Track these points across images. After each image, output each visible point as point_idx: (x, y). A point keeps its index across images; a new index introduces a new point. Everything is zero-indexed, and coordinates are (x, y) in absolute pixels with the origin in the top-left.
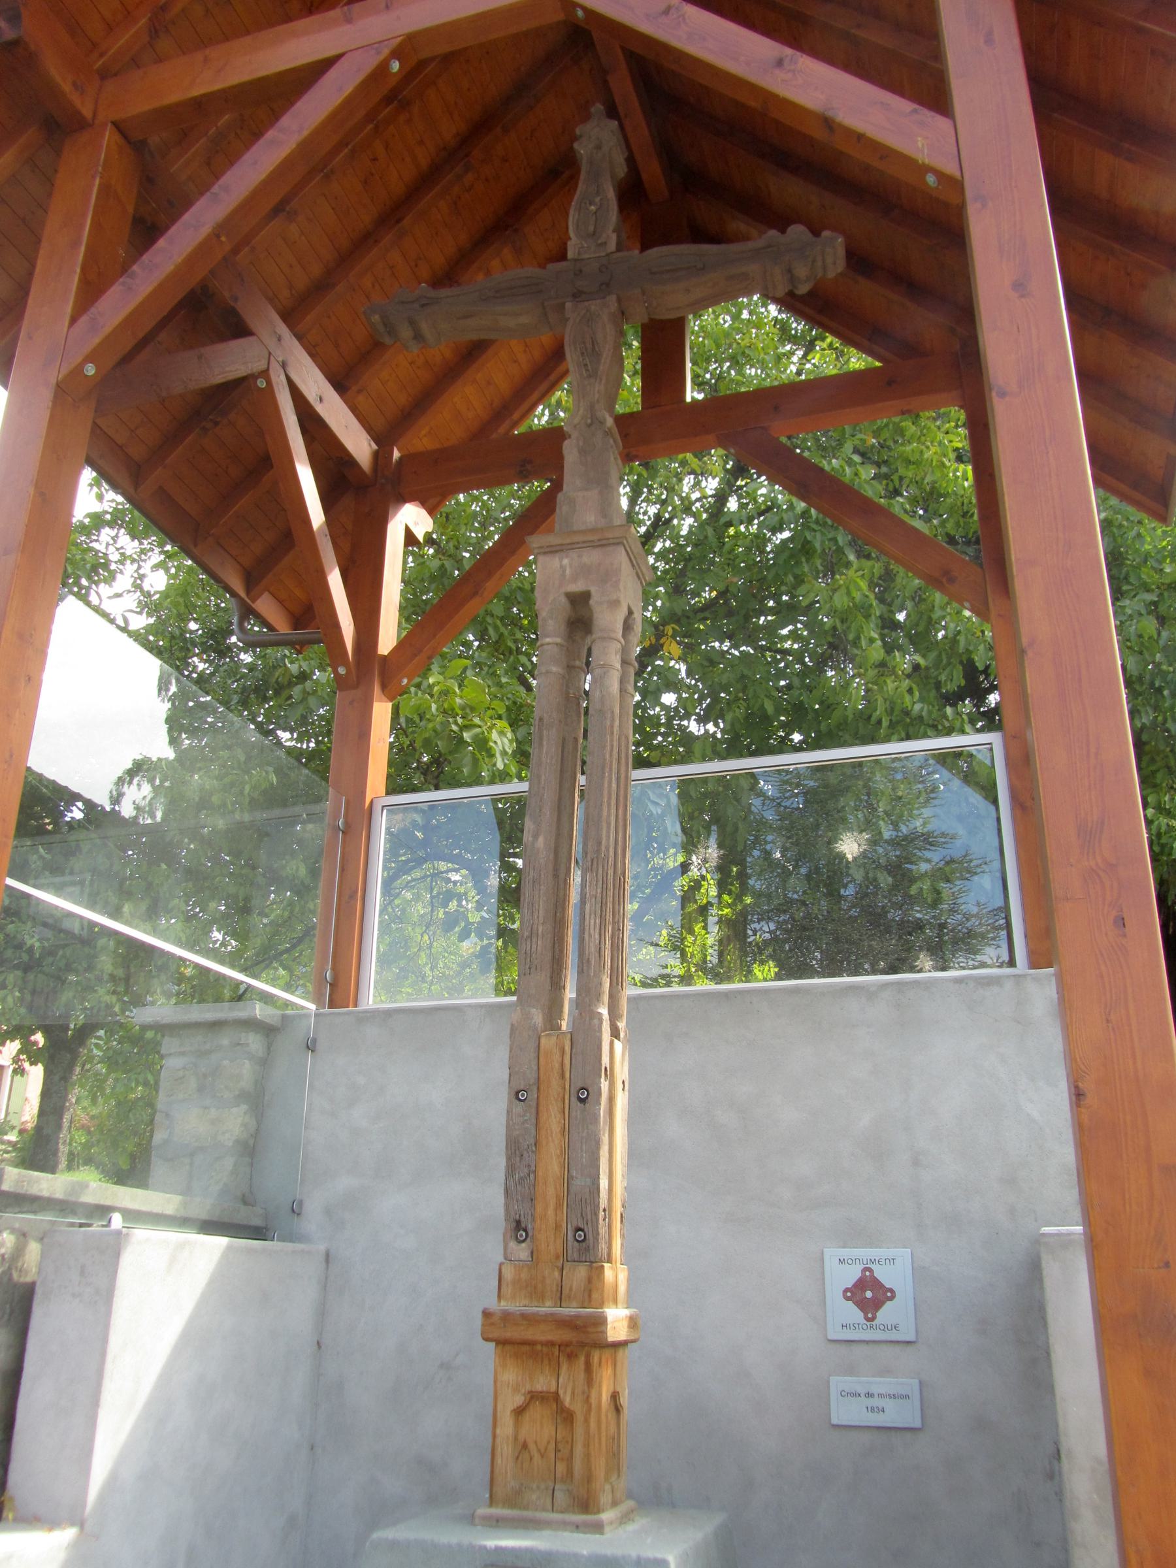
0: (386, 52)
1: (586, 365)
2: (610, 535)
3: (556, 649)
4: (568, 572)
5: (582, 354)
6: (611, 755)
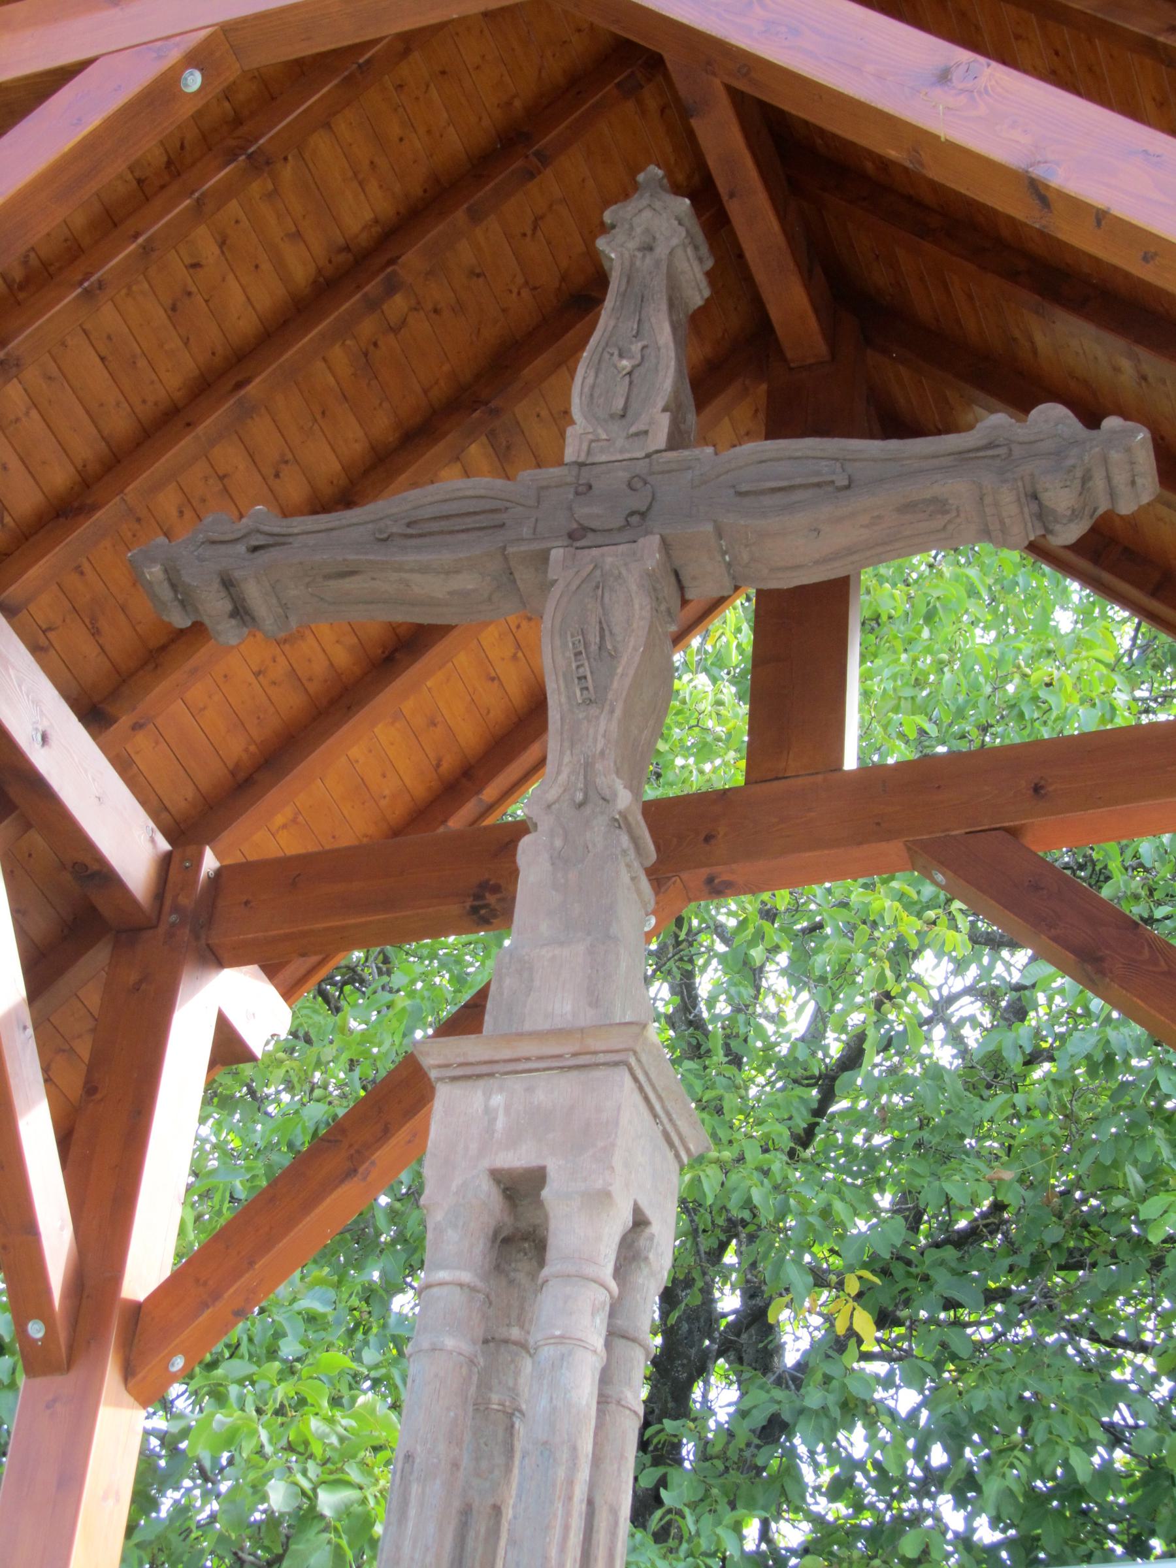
0: (175, 55)
1: (583, 678)
2: (600, 1045)
3: (457, 1297)
4: (500, 1124)
5: (578, 654)
6: (563, 1549)
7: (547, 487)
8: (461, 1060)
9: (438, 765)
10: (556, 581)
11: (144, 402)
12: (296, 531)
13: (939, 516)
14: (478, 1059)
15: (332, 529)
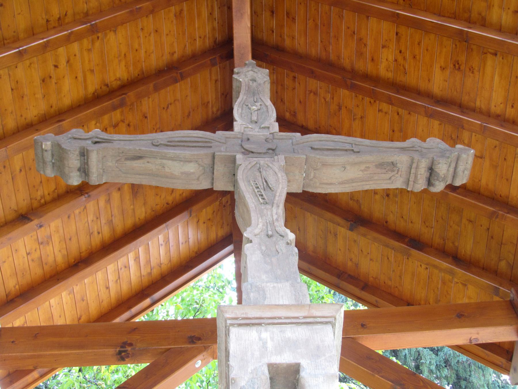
7: (229, 138)
8: (244, 316)
9: (80, 319)
10: (241, 165)
11: (21, 116)
12: (115, 139)
13: (390, 172)
14: (253, 316)
15: (132, 140)
